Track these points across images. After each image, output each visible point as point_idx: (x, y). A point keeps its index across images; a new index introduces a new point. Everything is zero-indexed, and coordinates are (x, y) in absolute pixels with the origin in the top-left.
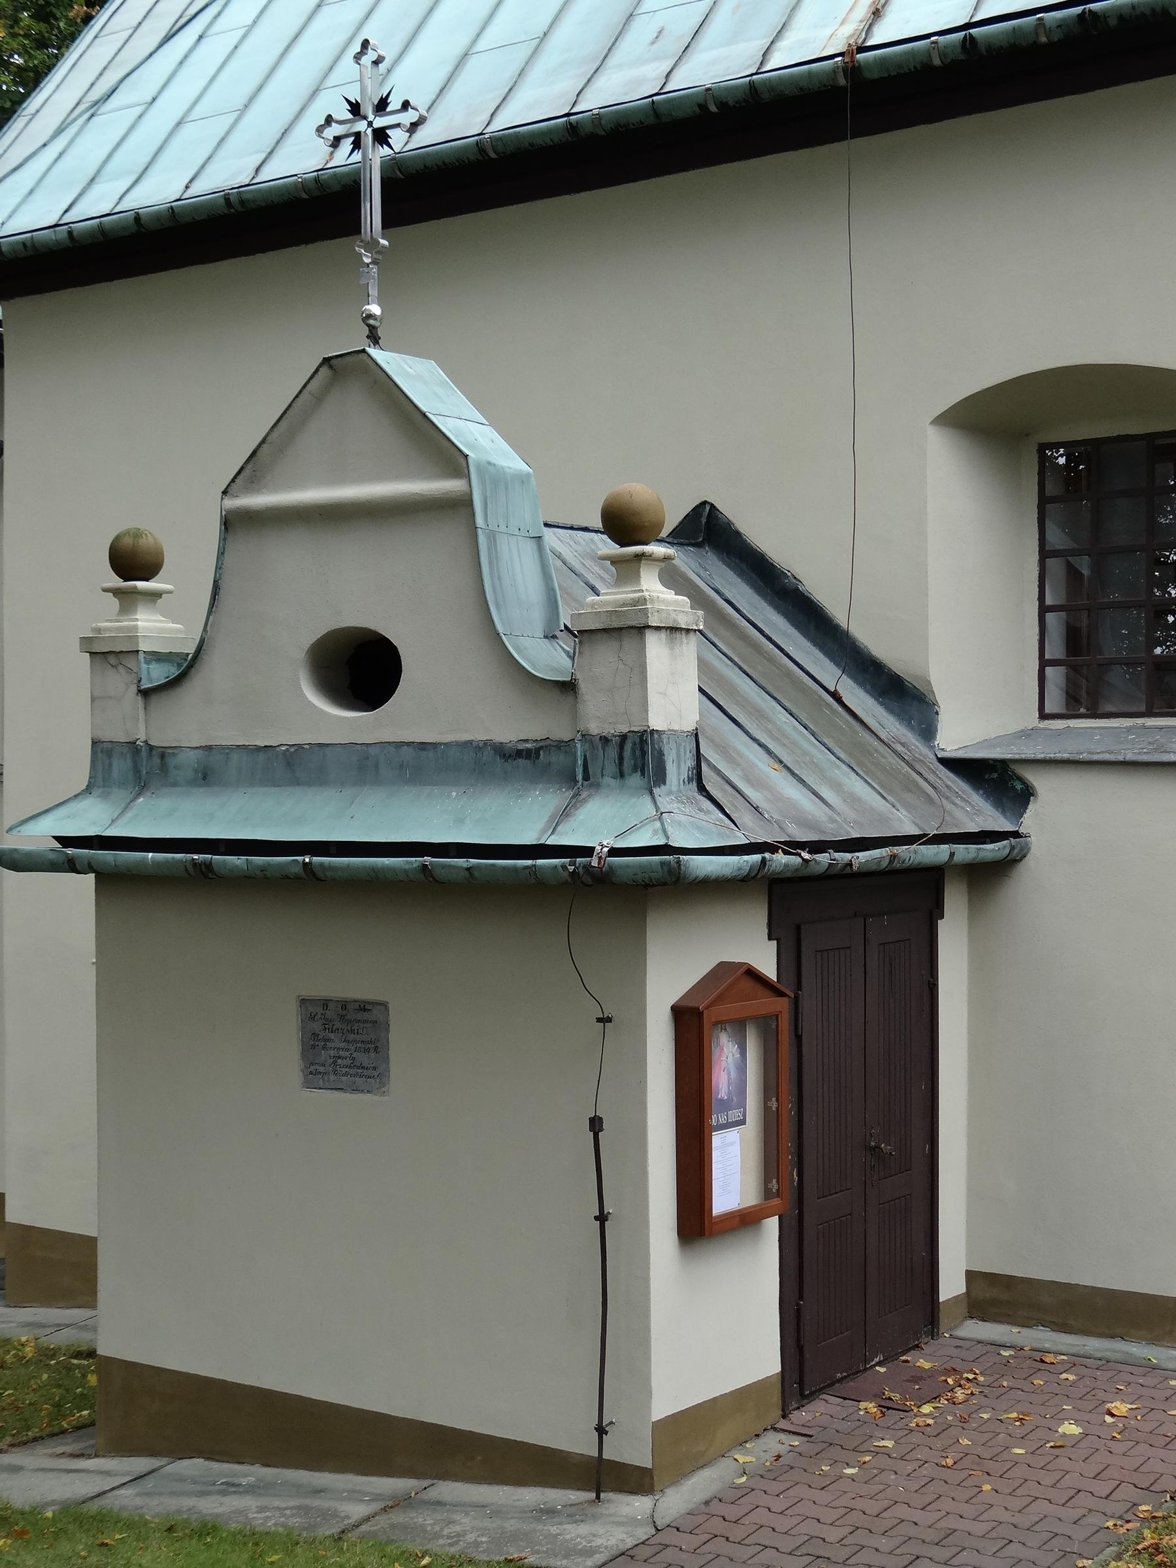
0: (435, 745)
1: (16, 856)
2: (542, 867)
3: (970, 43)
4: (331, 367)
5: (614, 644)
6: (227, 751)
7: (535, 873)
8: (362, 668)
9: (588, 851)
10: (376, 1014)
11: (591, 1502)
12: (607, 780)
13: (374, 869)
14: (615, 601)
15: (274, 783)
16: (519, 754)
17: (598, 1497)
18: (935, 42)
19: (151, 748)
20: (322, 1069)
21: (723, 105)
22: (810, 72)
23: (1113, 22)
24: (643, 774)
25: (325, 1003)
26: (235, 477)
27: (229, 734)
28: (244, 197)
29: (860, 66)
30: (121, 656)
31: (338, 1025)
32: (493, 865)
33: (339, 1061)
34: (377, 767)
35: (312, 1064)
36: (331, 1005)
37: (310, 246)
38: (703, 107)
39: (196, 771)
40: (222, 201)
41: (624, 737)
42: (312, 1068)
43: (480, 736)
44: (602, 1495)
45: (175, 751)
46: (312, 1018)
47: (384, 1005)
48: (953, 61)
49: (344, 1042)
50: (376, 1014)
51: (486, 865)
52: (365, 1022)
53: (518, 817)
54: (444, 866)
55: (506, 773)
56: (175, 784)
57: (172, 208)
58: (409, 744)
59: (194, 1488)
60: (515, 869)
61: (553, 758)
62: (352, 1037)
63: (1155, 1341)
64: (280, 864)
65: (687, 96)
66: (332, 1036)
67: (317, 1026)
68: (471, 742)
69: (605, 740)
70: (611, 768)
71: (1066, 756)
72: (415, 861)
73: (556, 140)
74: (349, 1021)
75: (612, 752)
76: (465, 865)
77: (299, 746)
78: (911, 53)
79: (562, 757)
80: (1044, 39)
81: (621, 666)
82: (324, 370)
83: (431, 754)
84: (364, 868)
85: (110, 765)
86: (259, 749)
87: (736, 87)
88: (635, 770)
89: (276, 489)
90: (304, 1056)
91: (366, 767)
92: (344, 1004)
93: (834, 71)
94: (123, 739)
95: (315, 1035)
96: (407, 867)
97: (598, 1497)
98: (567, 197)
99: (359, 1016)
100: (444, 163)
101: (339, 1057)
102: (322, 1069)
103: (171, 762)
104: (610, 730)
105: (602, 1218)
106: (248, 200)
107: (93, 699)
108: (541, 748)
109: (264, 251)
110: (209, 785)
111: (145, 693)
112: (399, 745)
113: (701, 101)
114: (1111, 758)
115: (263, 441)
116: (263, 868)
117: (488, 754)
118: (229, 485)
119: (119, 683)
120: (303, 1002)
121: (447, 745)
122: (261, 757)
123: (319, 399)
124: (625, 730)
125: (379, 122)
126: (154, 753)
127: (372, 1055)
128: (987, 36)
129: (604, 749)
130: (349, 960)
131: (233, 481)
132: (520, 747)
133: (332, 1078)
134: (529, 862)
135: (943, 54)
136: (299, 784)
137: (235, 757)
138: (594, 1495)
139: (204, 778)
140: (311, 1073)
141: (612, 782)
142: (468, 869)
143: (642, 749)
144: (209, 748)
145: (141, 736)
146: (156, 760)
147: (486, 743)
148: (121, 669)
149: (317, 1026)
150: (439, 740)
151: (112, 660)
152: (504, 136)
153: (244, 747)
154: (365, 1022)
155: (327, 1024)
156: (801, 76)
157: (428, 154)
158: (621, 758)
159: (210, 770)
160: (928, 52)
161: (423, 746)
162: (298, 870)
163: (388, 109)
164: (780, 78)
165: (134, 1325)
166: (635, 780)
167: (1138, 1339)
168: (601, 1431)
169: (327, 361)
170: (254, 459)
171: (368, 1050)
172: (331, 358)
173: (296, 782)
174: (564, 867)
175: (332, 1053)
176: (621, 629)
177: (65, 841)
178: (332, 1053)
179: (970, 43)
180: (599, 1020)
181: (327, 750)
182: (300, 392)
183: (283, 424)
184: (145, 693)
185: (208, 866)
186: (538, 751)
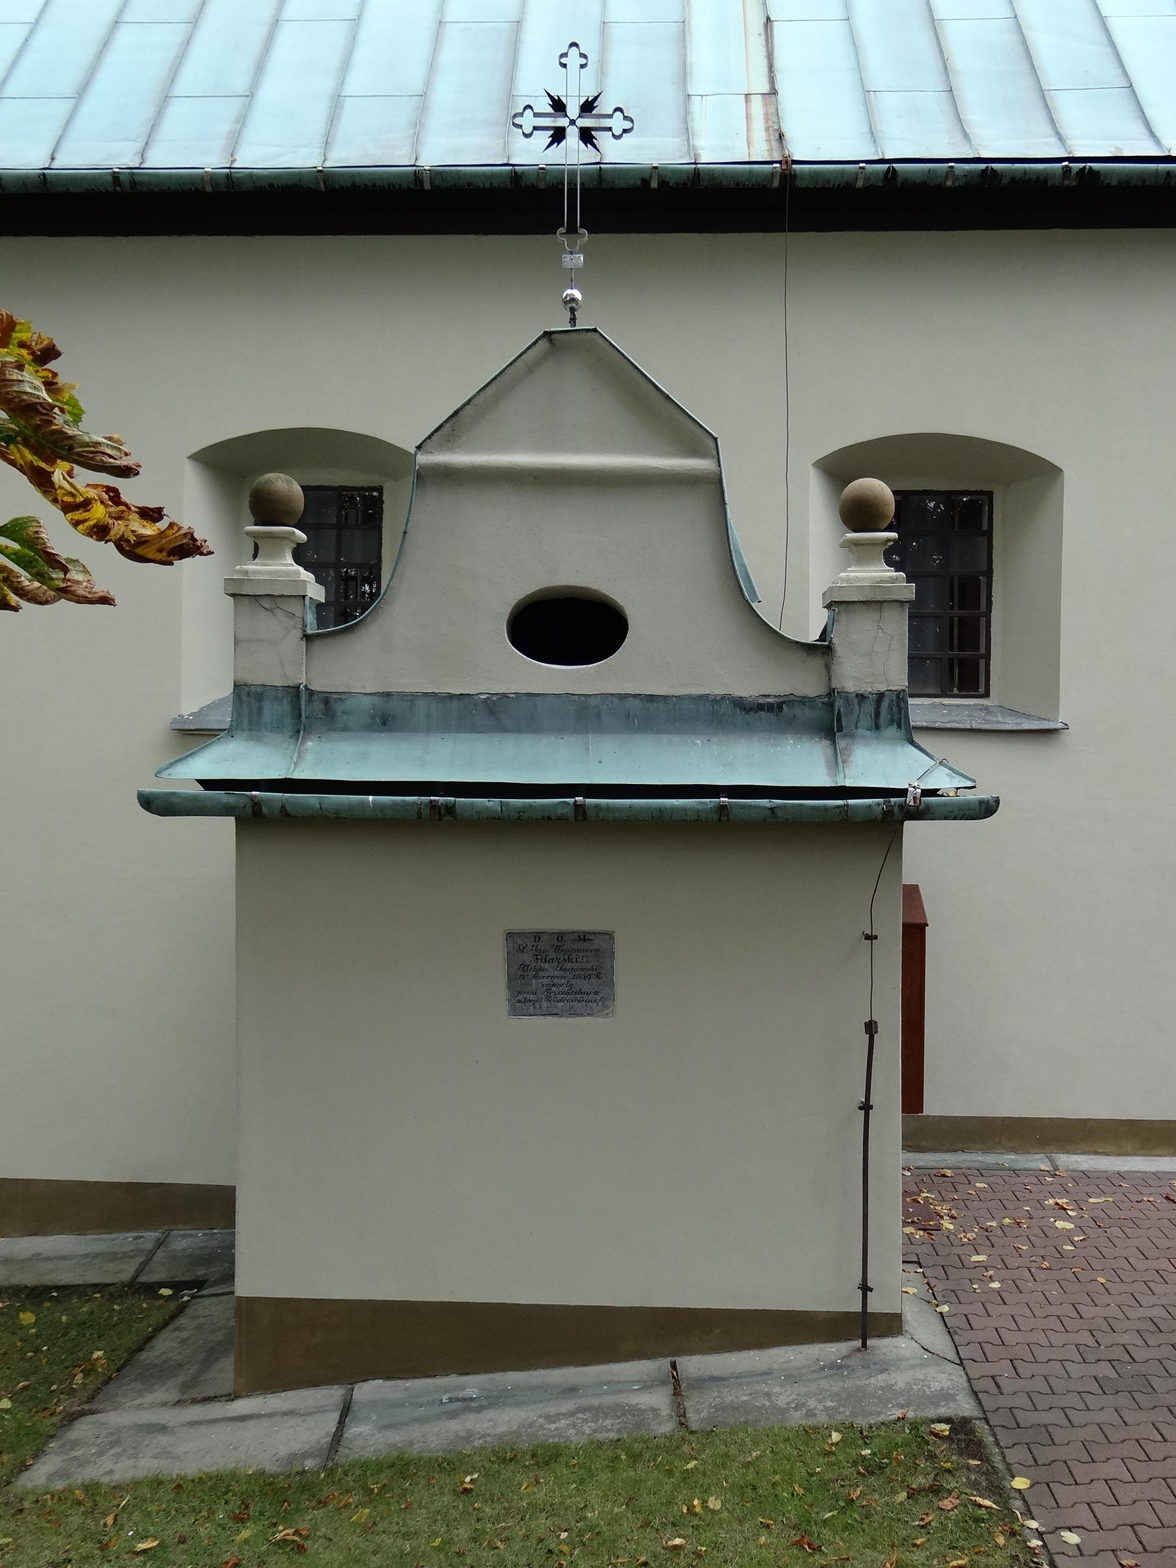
0: (665, 698)
1: (176, 800)
2: (854, 806)
3: (891, 175)
4: (551, 341)
5: (875, 616)
6: (412, 698)
7: (846, 813)
8: (571, 625)
9: (903, 793)
10: (598, 943)
11: (859, 1350)
12: (861, 731)
13: (660, 809)
14: (873, 578)
15: (474, 729)
16: (760, 707)
17: (864, 1345)
18: (863, 168)
19: (311, 693)
20: (532, 997)
21: (663, 183)
22: (751, 172)
23: (1005, 181)
24: (899, 727)
25: (537, 936)
26: (432, 434)
27: (412, 680)
28: (137, 179)
29: (795, 175)
30: (279, 601)
31: (552, 955)
32: (801, 805)
33: (554, 989)
34: (598, 716)
35: (520, 993)
36: (544, 937)
37: (184, 238)
38: (645, 182)
39: (373, 717)
40: (110, 178)
41: (881, 696)
42: (521, 997)
43: (717, 690)
44: (869, 1342)
45: (343, 697)
46: (521, 950)
47: (609, 936)
48: (872, 186)
49: (559, 971)
50: (598, 943)
51: (813, 808)
52: (585, 951)
53: (799, 763)
54: (744, 806)
55: (748, 724)
56: (345, 729)
57: (44, 174)
58: (635, 696)
59: (396, 1416)
60: (826, 809)
61: (798, 711)
62: (569, 965)
63: (987, 1150)
64: (543, 806)
65: (635, 170)
66: (546, 966)
67: (527, 958)
68: (707, 696)
69: (861, 697)
70: (866, 721)
71: (925, 724)
72: (710, 802)
73: (495, 184)
74: (565, 951)
75: (869, 708)
76: (768, 805)
77: (504, 696)
78: (842, 172)
79: (807, 712)
80: (949, 183)
81: (881, 634)
82: (544, 343)
83: (661, 705)
84: (649, 808)
85: (260, 709)
86: (451, 697)
87: (681, 171)
88: (891, 722)
89: (473, 451)
90: (510, 986)
91: (585, 717)
92: (560, 936)
93: (772, 174)
94: (279, 682)
95: (524, 966)
96: (700, 807)
97: (864, 1345)
98: (637, 235)
99: (578, 946)
100: (374, 185)
101: (554, 985)
102: (532, 997)
103: (339, 708)
104: (866, 688)
105: (866, 1107)
106: (141, 183)
107: (237, 641)
108: (784, 702)
109: (127, 234)
110: (390, 730)
111: (308, 638)
112: (623, 697)
113: (646, 176)
114: (961, 726)
115: (468, 403)
116: (521, 811)
117: (725, 707)
118: (425, 441)
119: (269, 625)
120: (510, 935)
121: (679, 698)
122: (455, 704)
123: (531, 369)
124: (883, 688)
125: (586, 122)
126: (315, 697)
127: (593, 980)
128: (907, 172)
129: (859, 705)
130: (564, 894)
131: (429, 437)
132: (761, 701)
133: (545, 1004)
134: (840, 802)
135: (867, 178)
136: (506, 731)
137: (422, 704)
138: (858, 1343)
139: (384, 723)
140: (519, 1001)
141: (868, 733)
142: (772, 809)
143: (898, 705)
144: (388, 695)
145: (304, 681)
146: (318, 706)
147: (723, 697)
148: (278, 613)
149: (527, 958)
150: (670, 693)
151: (267, 603)
152: (445, 171)
153: (434, 695)
154: (585, 951)
155: (539, 955)
156: (742, 172)
157: (359, 173)
158: (877, 713)
159: (389, 716)
160: (856, 176)
161: (651, 698)
162: (569, 812)
163: (594, 112)
164: (723, 170)
165: (273, 1263)
166: (892, 731)
167: (976, 1151)
168: (865, 1289)
169: (547, 335)
170: (453, 420)
171: (589, 977)
172: (554, 332)
173: (503, 729)
174: (878, 804)
175: (545, 981)
176: (882, 602)
177: (207, 784)
178: (545, 981)
179: (891, 175)
180: (876, 937)
181: (537, 699)
182: (515, 361)
183: (490, 390)
184: (308, 638)
185: (450, 809)
186: (780, 706)
